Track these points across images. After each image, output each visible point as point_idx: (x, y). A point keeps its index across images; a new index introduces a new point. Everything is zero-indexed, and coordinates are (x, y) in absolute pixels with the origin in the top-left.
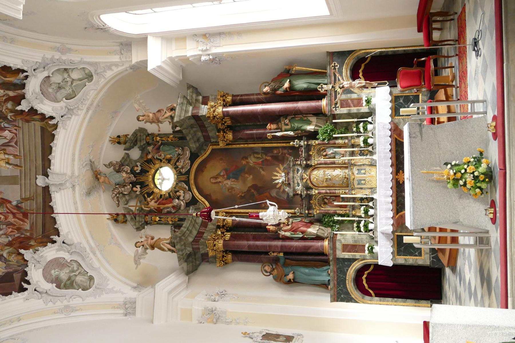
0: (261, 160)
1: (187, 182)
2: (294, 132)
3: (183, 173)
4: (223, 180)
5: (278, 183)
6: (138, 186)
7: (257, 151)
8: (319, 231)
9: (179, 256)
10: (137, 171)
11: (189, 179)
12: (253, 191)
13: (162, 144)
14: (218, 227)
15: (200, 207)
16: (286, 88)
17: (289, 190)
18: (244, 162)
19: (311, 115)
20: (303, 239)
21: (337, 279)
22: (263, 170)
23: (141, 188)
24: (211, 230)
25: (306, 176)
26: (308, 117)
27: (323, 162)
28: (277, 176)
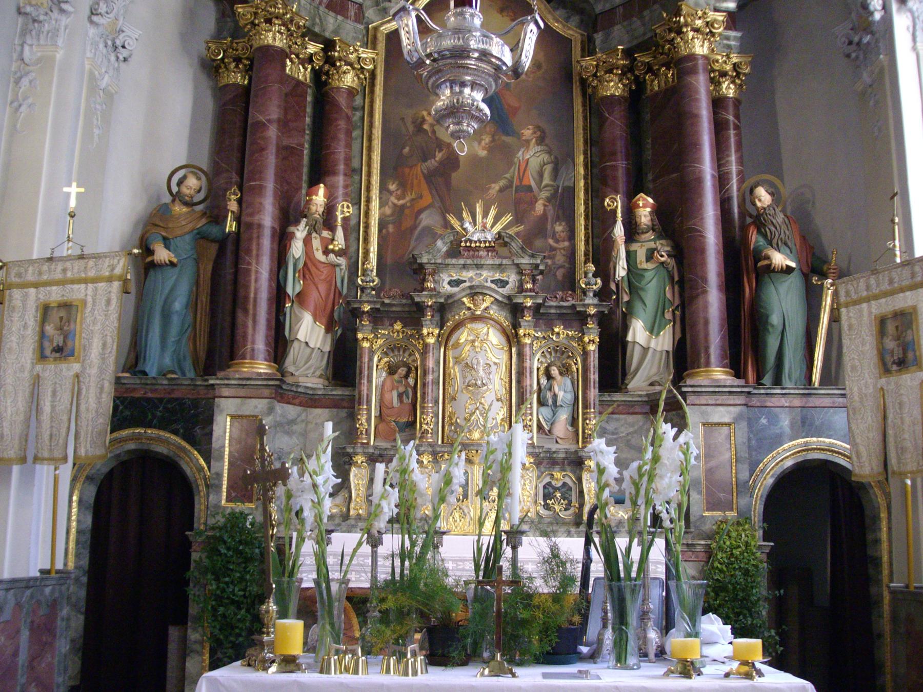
0: (533, 184)
2: (626, 279)
5: (461, 219)
7: (562, 171)
8: (303, 345)
12: (439, 156)
14: (329, 45)
16: (768, 258)
17: (439, 251)
18: (527, 133)
19: (678, 335)
20: (279, 296)
21: (148, 400)
22: (501, 190)
24: (320, 19)
26: (674, 326)
27: (527, 364)
28: (485, 215)
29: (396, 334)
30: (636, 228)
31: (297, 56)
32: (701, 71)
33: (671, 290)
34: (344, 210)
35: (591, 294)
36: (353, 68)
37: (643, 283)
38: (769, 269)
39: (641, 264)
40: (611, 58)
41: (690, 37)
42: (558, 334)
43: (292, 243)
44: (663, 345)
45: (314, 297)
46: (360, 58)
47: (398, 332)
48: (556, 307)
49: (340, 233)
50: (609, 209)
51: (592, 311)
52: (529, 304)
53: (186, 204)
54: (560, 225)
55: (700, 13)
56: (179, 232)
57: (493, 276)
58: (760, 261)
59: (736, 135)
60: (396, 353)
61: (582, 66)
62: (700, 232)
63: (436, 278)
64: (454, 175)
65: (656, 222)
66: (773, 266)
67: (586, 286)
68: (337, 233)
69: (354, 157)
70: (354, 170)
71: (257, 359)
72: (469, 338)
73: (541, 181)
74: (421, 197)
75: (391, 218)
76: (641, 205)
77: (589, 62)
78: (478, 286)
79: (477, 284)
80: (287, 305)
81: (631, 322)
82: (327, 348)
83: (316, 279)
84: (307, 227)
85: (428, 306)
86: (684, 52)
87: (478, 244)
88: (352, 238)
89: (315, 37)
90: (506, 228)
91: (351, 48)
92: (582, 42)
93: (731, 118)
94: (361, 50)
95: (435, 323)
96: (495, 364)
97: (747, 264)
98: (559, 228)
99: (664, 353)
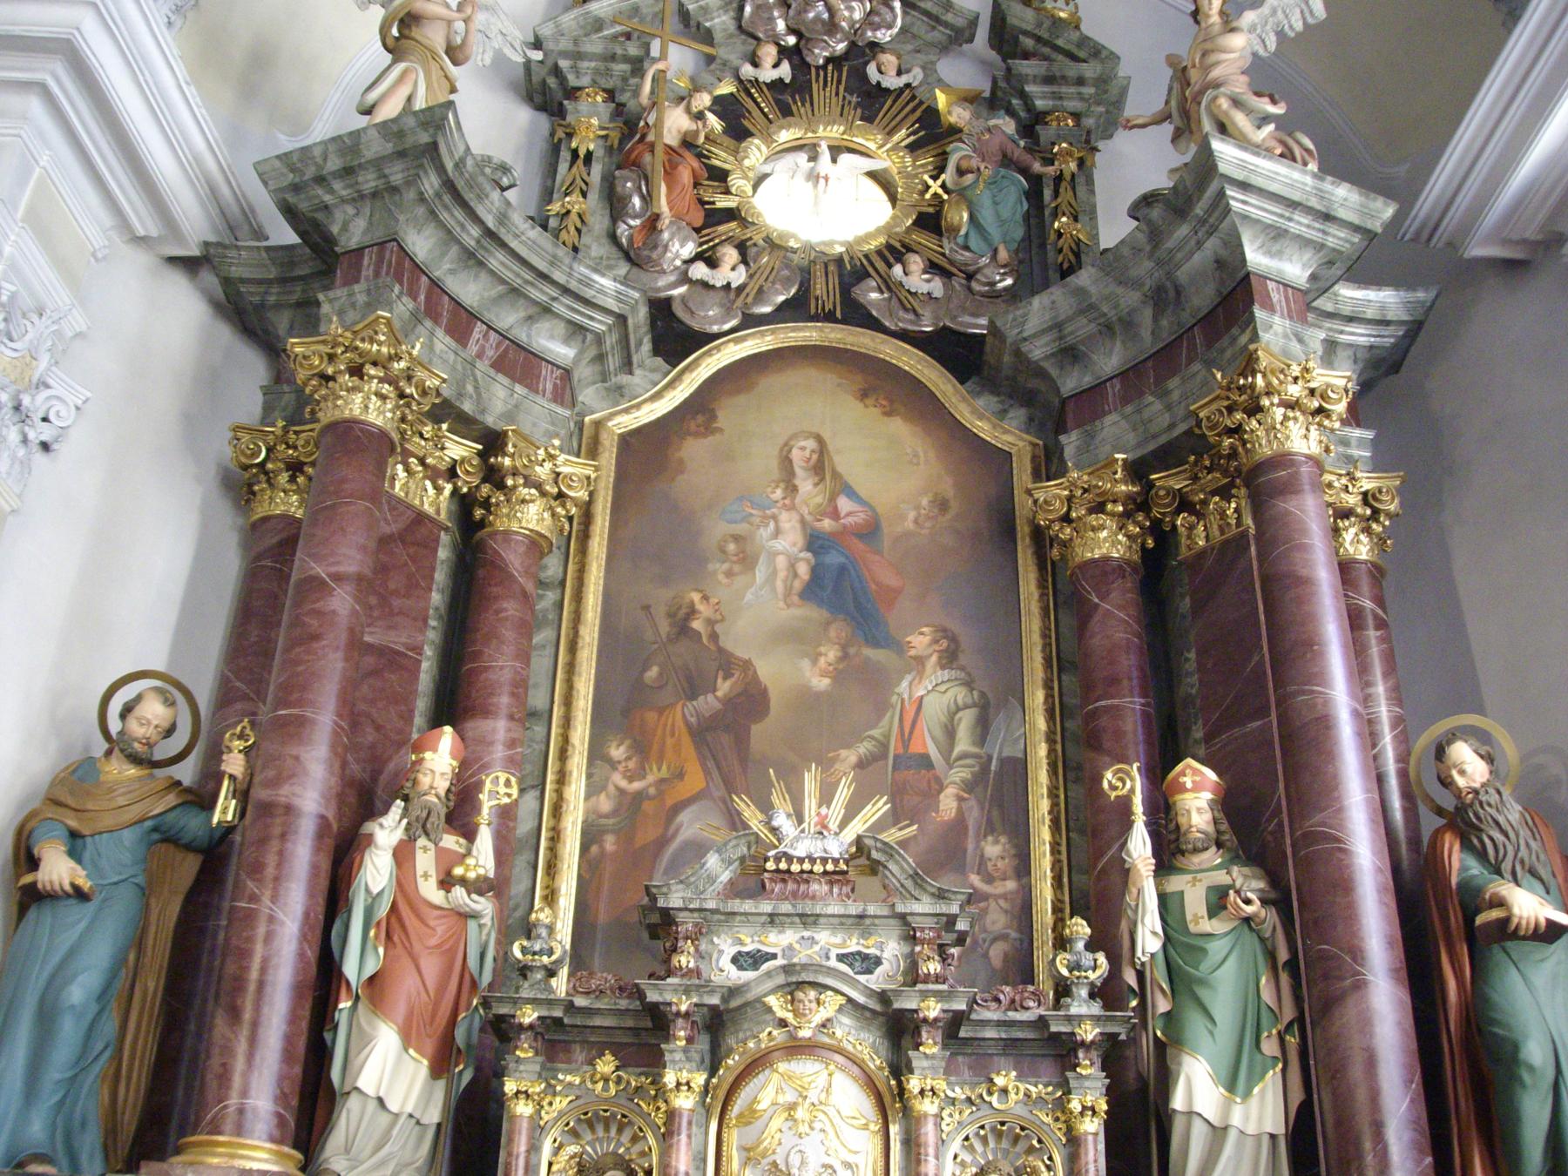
1: (795, 309)
2: (1160, 958)
3: (857, 292)
4: (805, 511)
5: (766, 808)
6: (785, 71)
7: (999, 722)
8: (372, 1106)
9: (317, 152)
10: (871, 70)
11: (815, 318)
12: (724, 687)
13: (1036, 181)
15: (638, 372)
16: (1500, 903)
17: (712, 880)
18: (920, 641)
19: (1297, 1097)
23: (777, 85)
24: (476, 388)
25: (818, 1019)
26: (1284, 1070)
28: (826, 798)
29: (600, 1084)
30: (1177, 839)
31: (422, 462)
32: (1307, 487)
33: (1272, 984)
34: (497, 790)
35: (1084, 992)
36: (543, 494)
37: (1205, 967)
38: (1505, 931)
39: (1197, 923)
40: (1101, 478)
41: (1279, 418)
42: (1004, 1091)
43: (367, 857)
44: (1260, 1119)
45: (408, 988)
46: (558, 474)
47: (606, 1080)
48: (1000, 1024)
49: (485, 841)
50: (1113, 795)
51: (1089, 1033)
52: (932, 1014)
53: (135, 759)
54: (996, 842)
55: (1296, 370)
56: (108, 821)
57: (843, 945)
58: (1478, 911)
59: (1382, 640)
60: (600, 1133)
61: (1035, 502)
62: (1338, 840)
63: (703, 947)
64: (756, 729)
65: (1225, 827)
66: (1515, 921)
67: (1070, 972)
68: (478, 841)
69: (536, 686)
70: (533, 714)
71: (250, 1136)
72: (781, 1099)
73: (951, 751)
74: (680, 775)
75: (611, 821)
76: (1189, 785)
77: (1053, 492)
78: (805, 967)
79: (804, 961)
80: (341, 1006)
81: (1180, 1064)
82: (433, 1115)
83: (417, 947)
84: (405, 821)
85: (678, 1014)
86: (1265, 450)
87: (807, 866)
88: (521, 862)
89: (465, 424)
90: (879, 826)
91: (541, 452)
92: (1034, 458)
93: (1368, 604)
94: (562, 458)
95: (696, 1057)
96: (848, 1165)
97: (1445, 919)
98: (994, 849)
99: (1266, 1141)
